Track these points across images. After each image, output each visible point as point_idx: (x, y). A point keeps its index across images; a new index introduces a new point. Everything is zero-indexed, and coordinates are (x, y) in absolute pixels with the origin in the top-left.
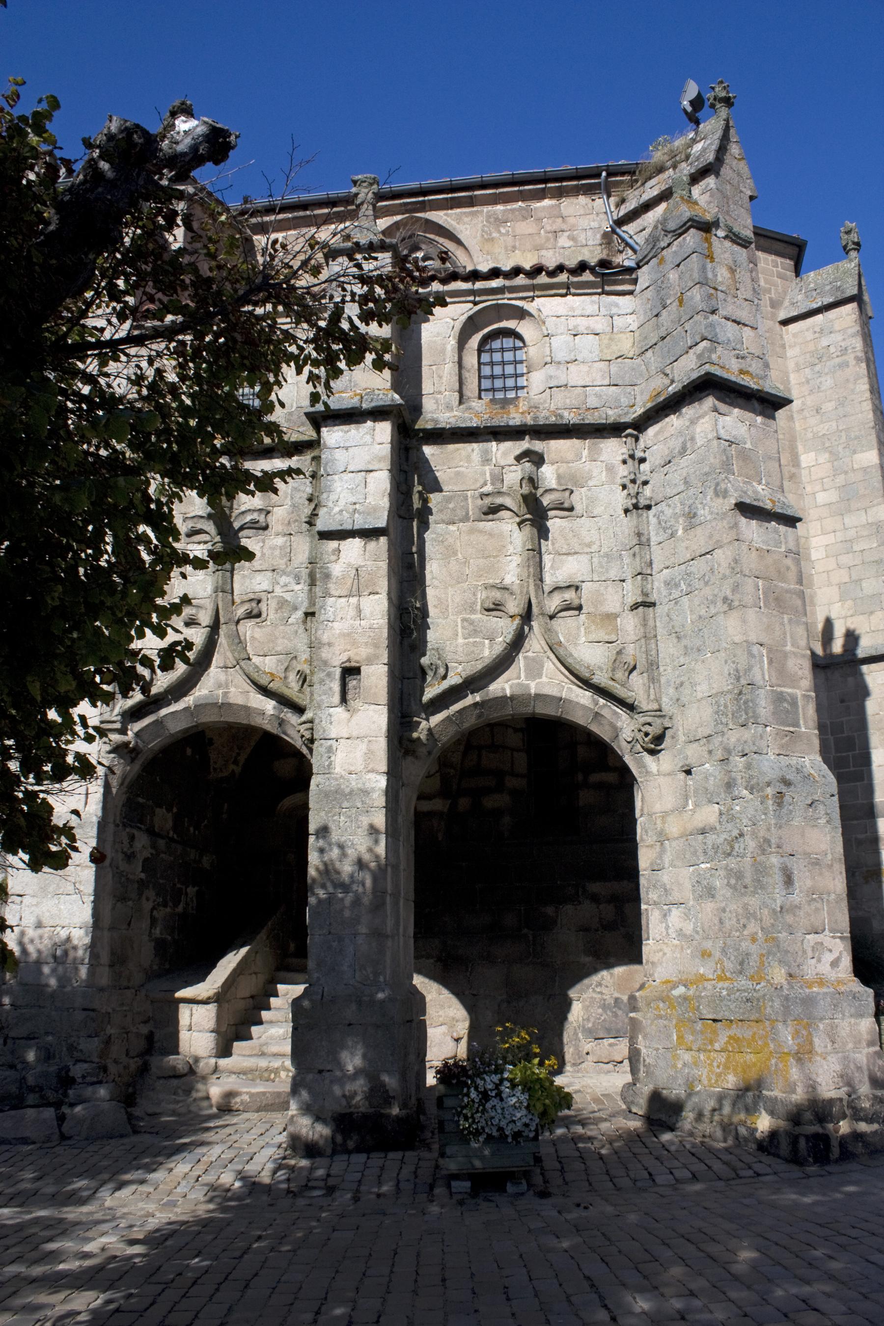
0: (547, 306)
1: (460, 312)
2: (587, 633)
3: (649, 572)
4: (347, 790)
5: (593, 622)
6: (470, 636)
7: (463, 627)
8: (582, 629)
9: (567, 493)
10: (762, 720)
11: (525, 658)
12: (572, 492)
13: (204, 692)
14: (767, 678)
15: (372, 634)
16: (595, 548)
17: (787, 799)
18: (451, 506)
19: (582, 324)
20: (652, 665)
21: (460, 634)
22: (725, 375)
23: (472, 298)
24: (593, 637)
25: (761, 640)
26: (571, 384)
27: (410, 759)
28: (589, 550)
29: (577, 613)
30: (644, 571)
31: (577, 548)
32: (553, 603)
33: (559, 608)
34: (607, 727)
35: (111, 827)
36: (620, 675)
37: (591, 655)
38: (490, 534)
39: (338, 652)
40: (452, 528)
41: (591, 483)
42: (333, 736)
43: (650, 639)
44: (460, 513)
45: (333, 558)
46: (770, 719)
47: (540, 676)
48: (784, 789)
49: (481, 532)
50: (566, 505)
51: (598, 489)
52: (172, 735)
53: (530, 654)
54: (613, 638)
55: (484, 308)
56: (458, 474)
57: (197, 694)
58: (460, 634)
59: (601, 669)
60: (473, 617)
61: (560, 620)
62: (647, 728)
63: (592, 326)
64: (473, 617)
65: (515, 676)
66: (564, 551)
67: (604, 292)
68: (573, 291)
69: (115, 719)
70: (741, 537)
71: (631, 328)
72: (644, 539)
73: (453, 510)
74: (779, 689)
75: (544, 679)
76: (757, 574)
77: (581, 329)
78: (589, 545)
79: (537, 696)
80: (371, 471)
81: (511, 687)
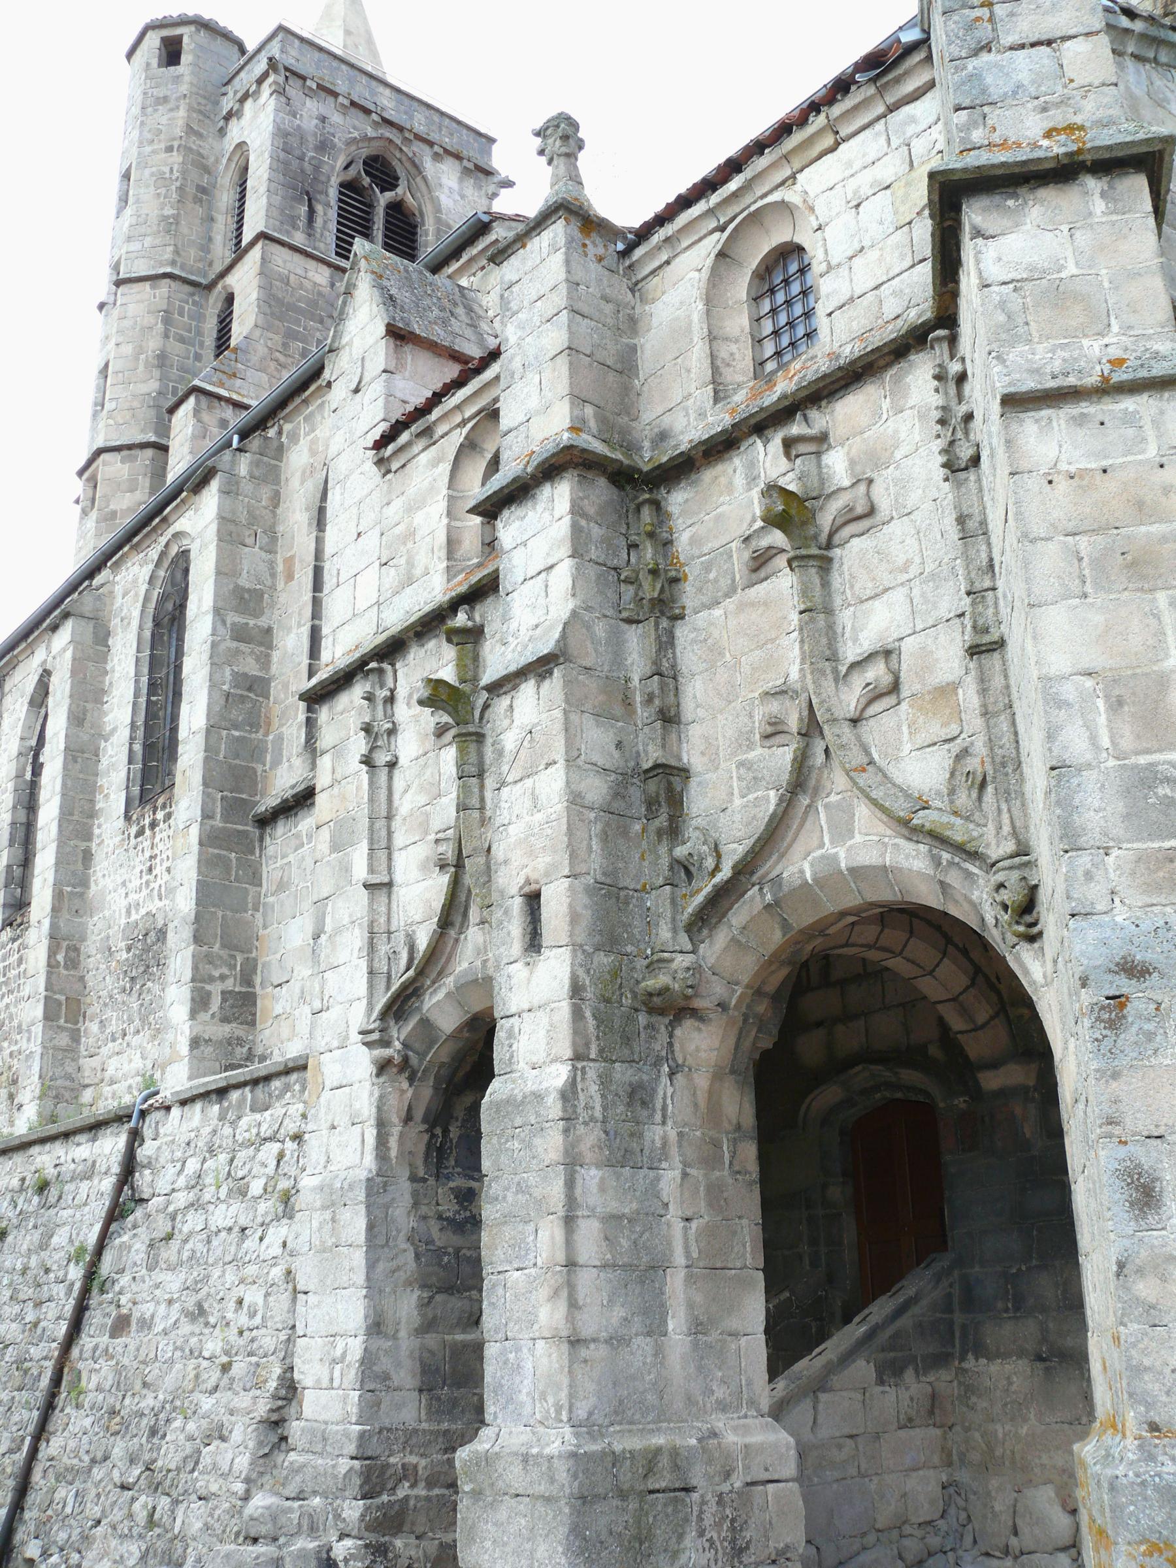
0: (817, 179)
1: (704, 253)
2: (913, 730)
3: (987, 584)
4: (519, 1098)
5: (920, 709)
6: (749, 790)
7: (739, 778)
8: (905, 729)
9: (862, 488)
10: (1092, 837)
11: (826, 806)
12: (870, 481)
13: (465, 965)
14: (1105, 742)
15: (549, 831)
16: (914, 570)
17: (1138, 1006)
18: (712, 576)
19: (864, 182)
20: (1004, 765)
21: (736, 791)
22: (1022, 156)
23: (713, 224)
24: (922, 738)
25: (1085, 664)
26: (858, 292)
27: (689, 1023)
28: (906, 577)
29: (892, 700)
30: (978, 586)
31: (887, 580)
32: (850, 698)
33: (863, 701)
34: (966, 906)
35: (403, 1190)
36: (964, 799)
37: (922, 771)
38: (766, 604)
39: (514, 873)
40: (718, 612)
41: (898, 455)
42: (513, 1010)
43: (997, 714)
44: (724, 583)
45: (506, 722)
46: (1118, 831)
47: (851, 833)
48: (1124, 985)
49: (752, 604)
50: (859, 510)
51: (909, 461)
52: (451, 1037)
53: (833, 798)
54: (954, 729)
55: (735, 229)
56: (718, 518)
57: (458, 969)
58: (736, 791)
59: (938, 793)
60: (751, 755)
61: (872, 722)
62: (1005, 895)
63: (879, 177)
64: (751, 755)
65: (816, 843)
66: (869, 593)
67: (892, 109)
68: (843, 133)
69: (372, 1027)
70: (1024, 465)
71: (939, 147)
72: (972, 525)
73: (716, 580)
74: (1143, 760)
75: (858, 838)
76: (1070, 526)
77: (866, 190)
78: (905, 569)
79: (852, 870)
80: (552, 567)
81: (812, 865)
